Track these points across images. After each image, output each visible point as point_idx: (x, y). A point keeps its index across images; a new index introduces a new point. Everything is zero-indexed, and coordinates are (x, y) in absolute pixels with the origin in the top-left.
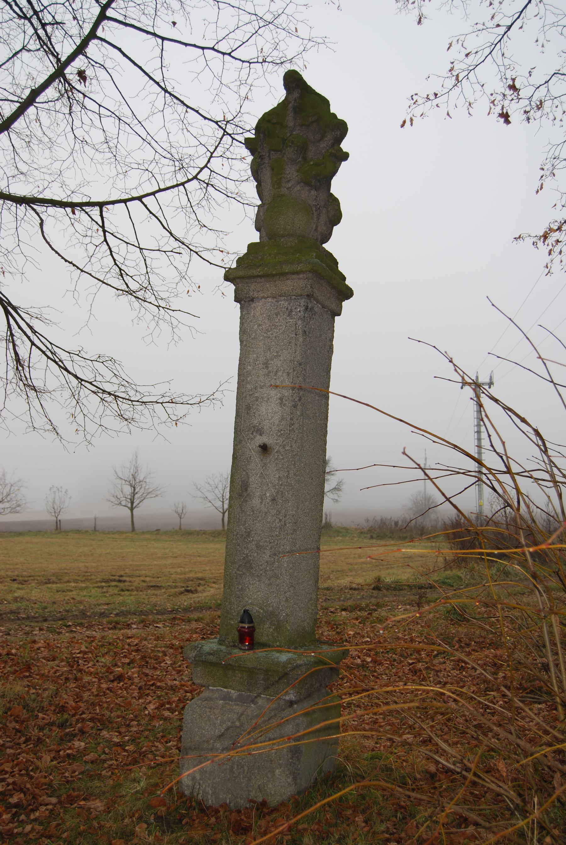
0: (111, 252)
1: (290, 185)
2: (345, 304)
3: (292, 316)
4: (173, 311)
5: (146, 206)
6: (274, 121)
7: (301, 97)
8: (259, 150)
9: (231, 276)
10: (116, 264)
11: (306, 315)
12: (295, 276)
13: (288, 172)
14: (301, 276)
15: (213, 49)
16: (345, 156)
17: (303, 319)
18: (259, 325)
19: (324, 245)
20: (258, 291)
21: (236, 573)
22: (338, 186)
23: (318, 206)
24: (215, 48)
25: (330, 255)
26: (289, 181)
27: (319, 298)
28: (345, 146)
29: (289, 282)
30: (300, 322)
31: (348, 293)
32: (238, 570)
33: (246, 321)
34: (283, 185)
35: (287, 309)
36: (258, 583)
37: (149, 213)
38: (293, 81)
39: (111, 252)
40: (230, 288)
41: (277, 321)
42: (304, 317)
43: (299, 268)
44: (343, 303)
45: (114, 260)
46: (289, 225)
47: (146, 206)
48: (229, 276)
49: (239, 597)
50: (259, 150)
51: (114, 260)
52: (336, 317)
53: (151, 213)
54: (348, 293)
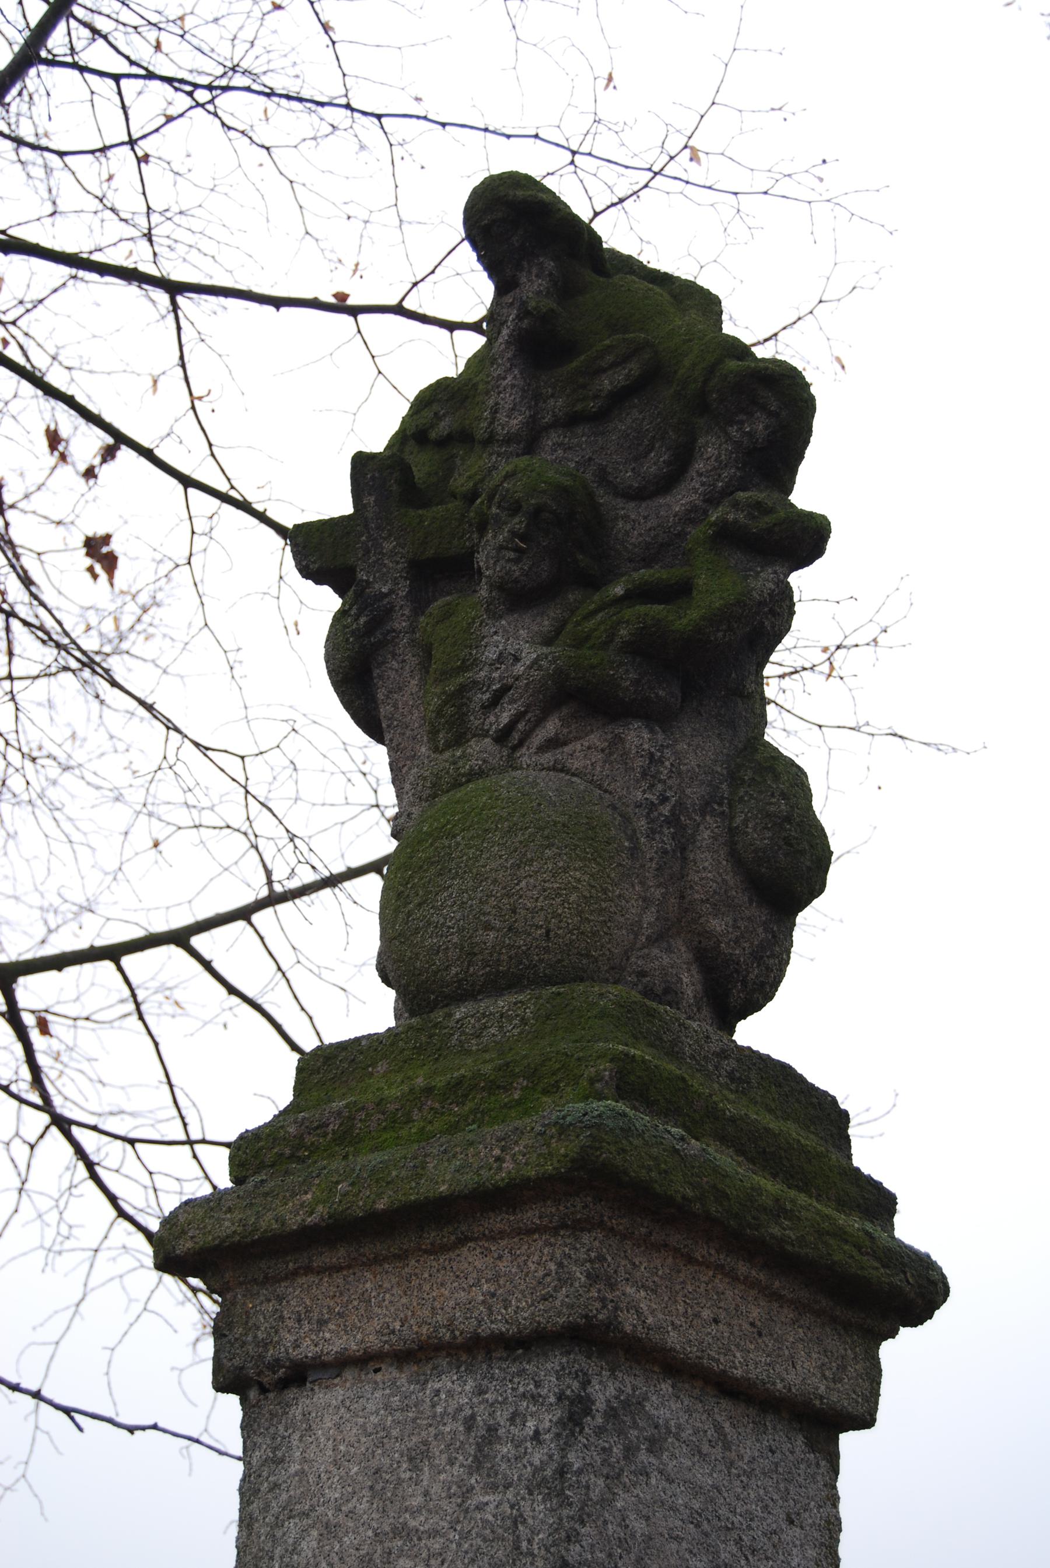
0: (90, 1166)
1: (505, 718)
2: (901, 1354)
3: (494, 1471)
4: (131, 1430)
5: (207, 965)
6: (444, 427)
7: (566, 289)
8: (362, 576)
9: (184, 1246)
10: (122, 1214)
11: (575, 1460)
12: (498, 1222)
13: (491, 654)
14: (531, 1216)
15: (398, 310)
16: (809, 538)
17: (555, 1483)
18: (330, 1530)
19: (752, 1033)
20: (322, 1323)
22: (802, 711)
23: (666, 810)
24: (407, 304)
25: (781, 1079)
26: (495, 701)
27: (673, 1339)
28: (807, 493)
29: (472, 1259)
30: (537, 1510)
31: (915, 1291)
33: (267, 1508)
34: (475, 722)
35: (470, 1423)
37: (223, 991)
38: (515, 223)
39: (90, 1166)
40: (182, 1319)
41: (417, 1501)
42: (562, 1472)
43: (508, 1165)
44: (887, 1350)
45: (113, 1199)
46: (488, 927)
47: (207, 965)
48: (184, 1248)
50: (362, 576)
51: (113, 1199)
52: (849, 1442)
53: (232, 990)
54: (915, 1291)
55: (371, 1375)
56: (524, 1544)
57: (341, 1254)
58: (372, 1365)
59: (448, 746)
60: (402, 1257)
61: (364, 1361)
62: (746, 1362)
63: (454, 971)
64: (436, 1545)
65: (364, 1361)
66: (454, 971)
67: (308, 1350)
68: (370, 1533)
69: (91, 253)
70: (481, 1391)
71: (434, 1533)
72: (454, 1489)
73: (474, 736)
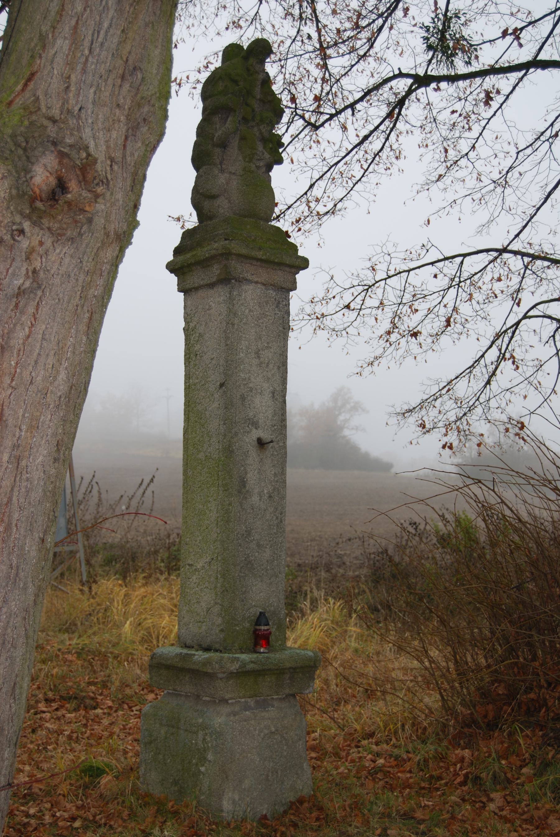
21: (239, 575)
32: (241, 572)
36: (260, 584)
49: (243, 601)
57: (259, 263)
61: (257, 283)
65: (257, 283)
67: (250, 277)
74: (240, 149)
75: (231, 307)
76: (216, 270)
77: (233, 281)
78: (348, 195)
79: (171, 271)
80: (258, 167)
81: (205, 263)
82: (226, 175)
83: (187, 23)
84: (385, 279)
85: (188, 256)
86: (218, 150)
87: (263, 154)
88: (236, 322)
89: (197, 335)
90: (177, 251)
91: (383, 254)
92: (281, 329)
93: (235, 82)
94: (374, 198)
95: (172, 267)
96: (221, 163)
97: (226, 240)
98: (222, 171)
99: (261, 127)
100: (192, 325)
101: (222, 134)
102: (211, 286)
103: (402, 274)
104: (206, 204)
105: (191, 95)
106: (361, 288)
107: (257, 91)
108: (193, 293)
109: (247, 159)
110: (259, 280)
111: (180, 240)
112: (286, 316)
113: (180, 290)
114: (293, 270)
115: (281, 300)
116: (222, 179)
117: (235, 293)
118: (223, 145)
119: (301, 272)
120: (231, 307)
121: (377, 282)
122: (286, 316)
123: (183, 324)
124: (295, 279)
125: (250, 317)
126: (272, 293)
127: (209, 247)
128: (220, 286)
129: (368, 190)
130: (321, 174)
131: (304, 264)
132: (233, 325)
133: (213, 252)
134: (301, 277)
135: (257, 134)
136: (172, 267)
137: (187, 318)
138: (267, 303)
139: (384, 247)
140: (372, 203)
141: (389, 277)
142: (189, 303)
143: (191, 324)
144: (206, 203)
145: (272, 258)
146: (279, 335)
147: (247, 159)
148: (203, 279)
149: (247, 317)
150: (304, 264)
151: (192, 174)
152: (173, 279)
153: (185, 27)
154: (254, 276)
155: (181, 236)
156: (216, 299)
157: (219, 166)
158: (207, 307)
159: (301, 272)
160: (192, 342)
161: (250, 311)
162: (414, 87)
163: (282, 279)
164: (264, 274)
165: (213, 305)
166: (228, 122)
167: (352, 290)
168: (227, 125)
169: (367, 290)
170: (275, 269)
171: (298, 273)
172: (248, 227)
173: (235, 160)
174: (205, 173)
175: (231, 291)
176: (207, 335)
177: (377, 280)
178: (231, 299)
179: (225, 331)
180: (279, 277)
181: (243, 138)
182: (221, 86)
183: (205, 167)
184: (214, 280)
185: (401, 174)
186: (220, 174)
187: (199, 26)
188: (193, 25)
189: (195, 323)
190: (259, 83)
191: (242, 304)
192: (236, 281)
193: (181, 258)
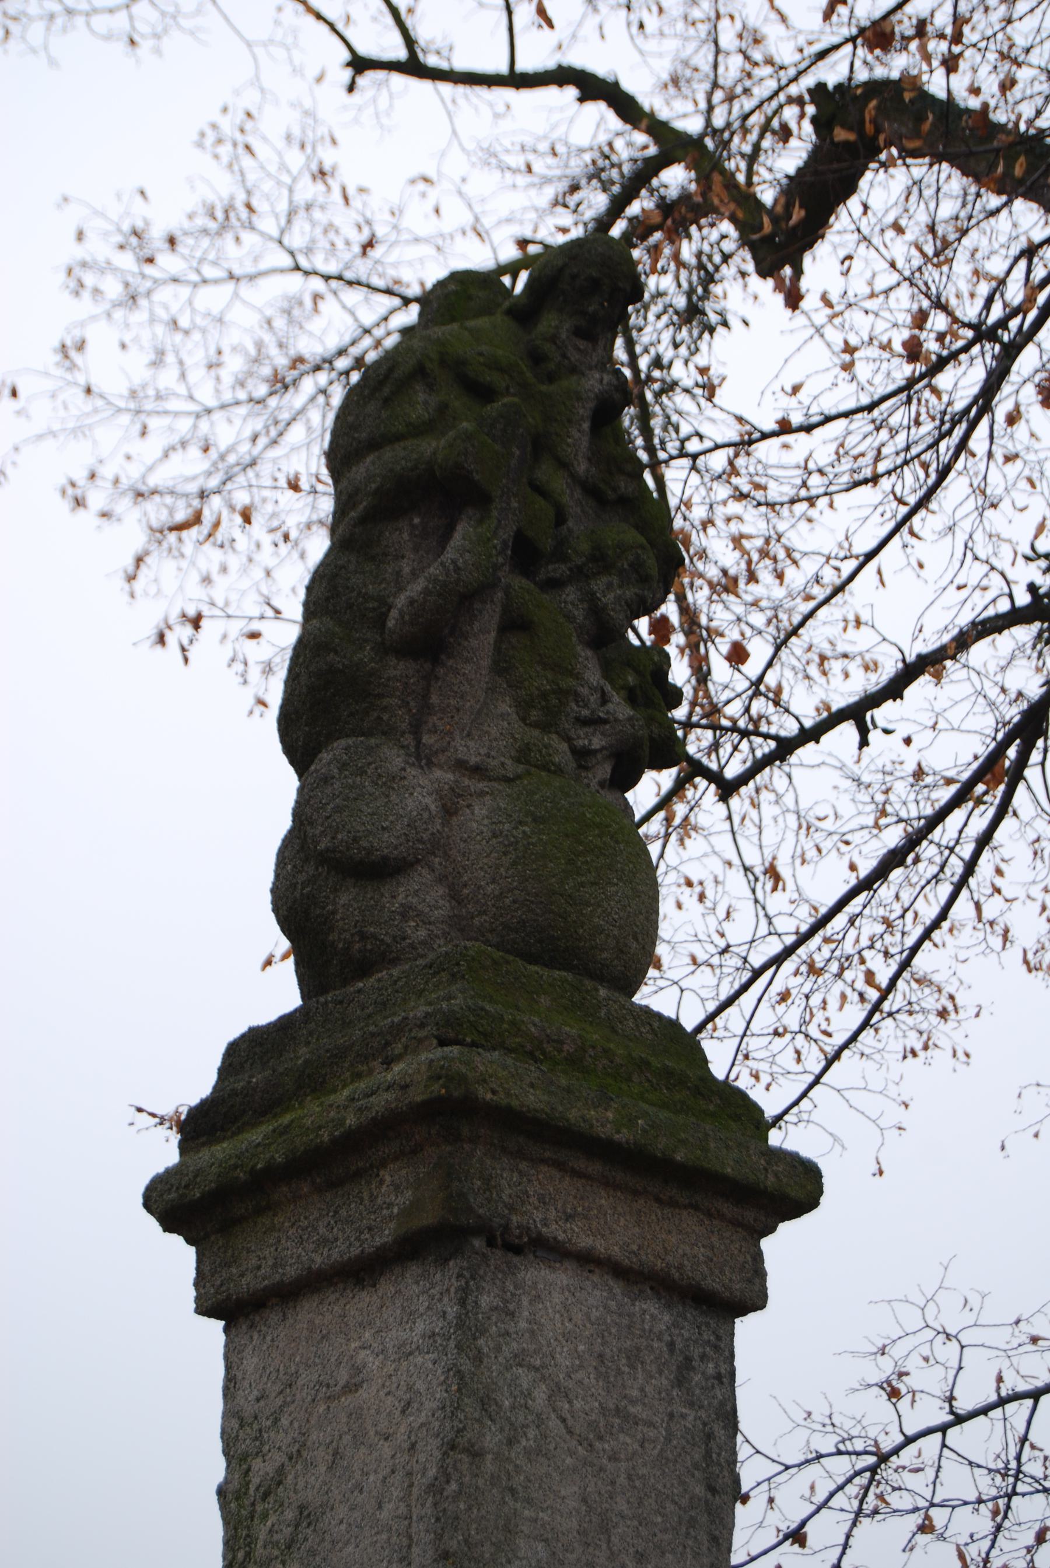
12: (727, 1208)
55: (585, 1274)
56: (714, 1456)
57: (595, 1168)
58: (592, 1267)
59: (535, 725)
60: (636, 1193)
61: (587, 1260)
62: (345, 1248)
63: (605, 955)
64: (652, 1433)
65: (587, 1260)
66: (605, 955)
67: (556, 1231)
68: (597, 1404)
69: (1027, 421)
70: (676, 1325)
71: (651, 1424)
72: (663, 1394)
73: (557, 733)
74: (501, 667)
75: (466, 1365)
76: (392, 1200)
77: (478, 1243)
78: (805, 1104)
79: (169, 1224)
80: (582, 755)
81: (333, 1165)
82: (438, 773)
83: (203, 565)
84: (943, 1429)
85: (256, 1135)
86: (398, 669)
87: (604, 700)
88: (491, 1439)
89: (290, 1515)
90: (197, 1127)
91: (929, 1334)
92: (699, 1490)
93: (481, 392)
94: (898, 1114)
95: (171, 1203)
96: (416, 729)
97: (443, 1043)
98: (424, 759)
99: (598, 585)
100: (262, 1469)
101: (426, 592)
102: (362, 1272)
103: (1010, 1408)
104: (347, 902)
105: (239, 667)
106: (842, 1466)
107: (578, 440)
108: (274, 1317)
109: (535, 715)
110: (600, 1246)
111: (212, 1078)
112: (720, 1433)
113: (206, 1308)
114: (750, 1215)
115: (696, 1352)
116: (421, 792)
117: (485, 1301)
118: (430, 643)
119: (784, 1227)
120: (466, 1365)
121: (909, 1440)
122: (720, 1433)
123: (216, 1469)
124: (758, 1257)
125: (554, 1423)
126: (654, 1313)
127: (362, 1085)
128: (414, 1269)
129: (876, 1084)
130: (711, 1007)
131: (798, 1188)
132: (475, 1454)
133: (381, 1102)
134: (784, 1248)
135: (579, 614)
136: (171, 1203)
137: (240, 1437)
138: (634, 1357)
139: (931, 1310)
140: (892, 1134)
141: (960, 1419)
142: (250, 1363)
143: (257, 1464)
144: (344, 899)
145: (661, 1144)
146: (692, 1522)
147: (535, 715)
148: (324, 1242)
149: (540, 1421)
150: (798, 1188)
151: (283, 784)
152: (180, 1256)
153: (195, 577)
154: (576, 1226)
155: (217, 1061)
156: (391, 1344)
157: (408, 740)
158: (343, 1376)
159: (785, 1228)
160: (259, 1551)
161: (557, 1391)
162: (1012, 752)
163: (701, 1252)
164: (616, 1225)
165: (373, 1363)
166: (457, 538)
167: (814, 1471)
168: (450, 554)
169: (873, 1470)
170: (673, 1204)
171: (772, 1229)
172: (544, 1001)
173: (483, 723)
174: (343, 766)
175: (465, 1290)
176: (342, 1511)
177: (910, 1431)
178: (467, 1330)
179: (435, 1489)
180: (682, 1241)
181: (516, 624)
182: (420, 404)
183: (343, 742)
184: (386, 1236)
185: (960, 1067)
186: (412, 771)
187: (244, 571)
188: (224, 569)
189: (279, 1458)
190: (584, 410)
191: (519, 1359)
192: (491, 1243)
193: (219, 1152)
